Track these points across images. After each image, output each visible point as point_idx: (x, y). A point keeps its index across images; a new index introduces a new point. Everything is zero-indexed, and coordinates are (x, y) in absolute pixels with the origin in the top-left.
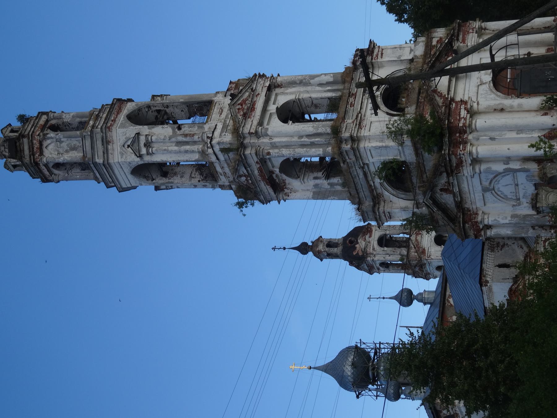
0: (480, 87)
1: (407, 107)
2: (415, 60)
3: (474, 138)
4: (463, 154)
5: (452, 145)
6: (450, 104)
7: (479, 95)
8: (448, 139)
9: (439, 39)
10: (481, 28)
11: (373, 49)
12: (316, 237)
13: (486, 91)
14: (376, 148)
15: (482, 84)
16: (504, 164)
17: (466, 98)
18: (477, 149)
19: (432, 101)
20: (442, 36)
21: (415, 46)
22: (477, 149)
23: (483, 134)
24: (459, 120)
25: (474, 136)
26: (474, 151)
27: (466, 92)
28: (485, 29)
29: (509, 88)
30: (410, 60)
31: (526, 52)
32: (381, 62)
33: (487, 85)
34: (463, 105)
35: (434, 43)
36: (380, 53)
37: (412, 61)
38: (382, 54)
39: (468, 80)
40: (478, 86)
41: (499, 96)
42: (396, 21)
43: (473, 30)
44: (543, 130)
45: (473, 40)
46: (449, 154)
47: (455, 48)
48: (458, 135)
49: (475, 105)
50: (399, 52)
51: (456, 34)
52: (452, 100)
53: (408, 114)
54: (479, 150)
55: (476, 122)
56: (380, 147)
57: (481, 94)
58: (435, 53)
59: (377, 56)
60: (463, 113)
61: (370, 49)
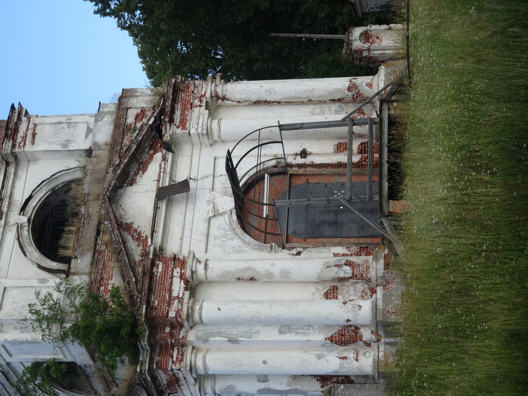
0: (213, 222)
1: (76, 257)
2: (94, 153)
3: (198, 338)
4: (179, 370)
5: (158, 349)
6: (153, 264)
7: (211, 239)
8: (149, 342)
9: (139, 111)
10: (216, 97)
11: (16, 124)
12: (120, 93)
13: (225, 230)
14: (14, 343)
15: (216, 214)
16: (259, 381)
17: (185, 253)
18: (204, 358)
19: (121, 251)
20: (144, 106)
21: (96, 121)
22: (204, 358)
23: (215, 329)
24: (169, 304)
25: (200, 334)
26: (199, 364)
27: (186, 241)
28: (224, 98)
29: (266, 233)
30: (86, 151)
31: (299, 150)
32: (31, 153)
33: (226, 217)
34: (178, 269)
35: (131, 120)
36: (30, 132)
37: (89, 152)
38: (34, 135)
39: (190, 206)
40: (210, 219)
41: (248, 244)
42: (96, 12)
43: (201, 101)
44: (330, 326)
45: (201, 122)
46: (150, 369)
47: (166, 138)
48: (168, 330)
49: (200, 268)
50: (66, 133)
51: (168, 109)
52: (159, 253)
53: (76, 274)
54: (208, 362)
55: (201, 309)
56: (21, 343)
57: (215, 237)
58: (129, 148)
59: (24, 138)
60: (178, 287)
61: (11, 126)
